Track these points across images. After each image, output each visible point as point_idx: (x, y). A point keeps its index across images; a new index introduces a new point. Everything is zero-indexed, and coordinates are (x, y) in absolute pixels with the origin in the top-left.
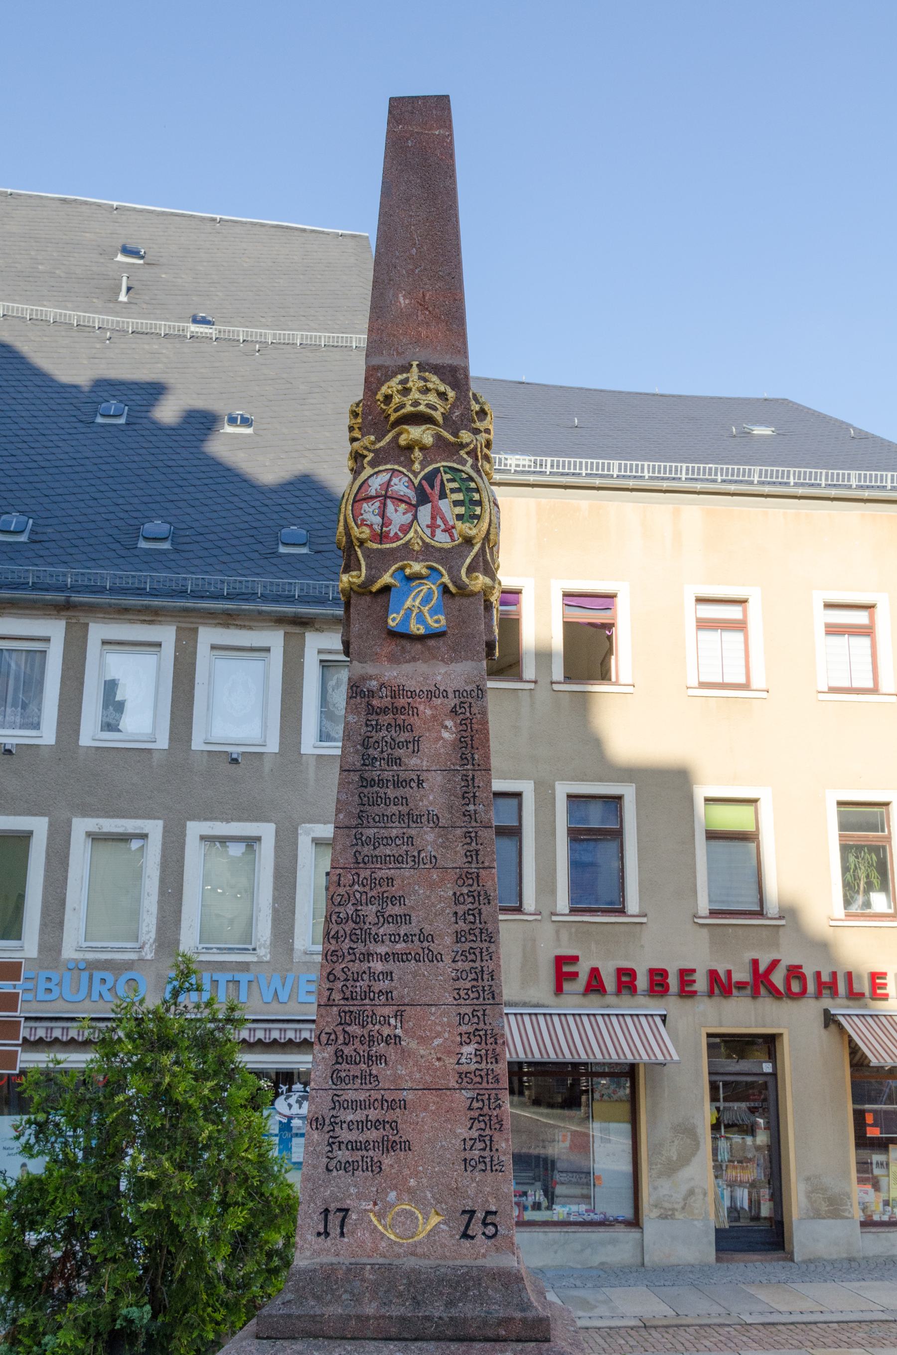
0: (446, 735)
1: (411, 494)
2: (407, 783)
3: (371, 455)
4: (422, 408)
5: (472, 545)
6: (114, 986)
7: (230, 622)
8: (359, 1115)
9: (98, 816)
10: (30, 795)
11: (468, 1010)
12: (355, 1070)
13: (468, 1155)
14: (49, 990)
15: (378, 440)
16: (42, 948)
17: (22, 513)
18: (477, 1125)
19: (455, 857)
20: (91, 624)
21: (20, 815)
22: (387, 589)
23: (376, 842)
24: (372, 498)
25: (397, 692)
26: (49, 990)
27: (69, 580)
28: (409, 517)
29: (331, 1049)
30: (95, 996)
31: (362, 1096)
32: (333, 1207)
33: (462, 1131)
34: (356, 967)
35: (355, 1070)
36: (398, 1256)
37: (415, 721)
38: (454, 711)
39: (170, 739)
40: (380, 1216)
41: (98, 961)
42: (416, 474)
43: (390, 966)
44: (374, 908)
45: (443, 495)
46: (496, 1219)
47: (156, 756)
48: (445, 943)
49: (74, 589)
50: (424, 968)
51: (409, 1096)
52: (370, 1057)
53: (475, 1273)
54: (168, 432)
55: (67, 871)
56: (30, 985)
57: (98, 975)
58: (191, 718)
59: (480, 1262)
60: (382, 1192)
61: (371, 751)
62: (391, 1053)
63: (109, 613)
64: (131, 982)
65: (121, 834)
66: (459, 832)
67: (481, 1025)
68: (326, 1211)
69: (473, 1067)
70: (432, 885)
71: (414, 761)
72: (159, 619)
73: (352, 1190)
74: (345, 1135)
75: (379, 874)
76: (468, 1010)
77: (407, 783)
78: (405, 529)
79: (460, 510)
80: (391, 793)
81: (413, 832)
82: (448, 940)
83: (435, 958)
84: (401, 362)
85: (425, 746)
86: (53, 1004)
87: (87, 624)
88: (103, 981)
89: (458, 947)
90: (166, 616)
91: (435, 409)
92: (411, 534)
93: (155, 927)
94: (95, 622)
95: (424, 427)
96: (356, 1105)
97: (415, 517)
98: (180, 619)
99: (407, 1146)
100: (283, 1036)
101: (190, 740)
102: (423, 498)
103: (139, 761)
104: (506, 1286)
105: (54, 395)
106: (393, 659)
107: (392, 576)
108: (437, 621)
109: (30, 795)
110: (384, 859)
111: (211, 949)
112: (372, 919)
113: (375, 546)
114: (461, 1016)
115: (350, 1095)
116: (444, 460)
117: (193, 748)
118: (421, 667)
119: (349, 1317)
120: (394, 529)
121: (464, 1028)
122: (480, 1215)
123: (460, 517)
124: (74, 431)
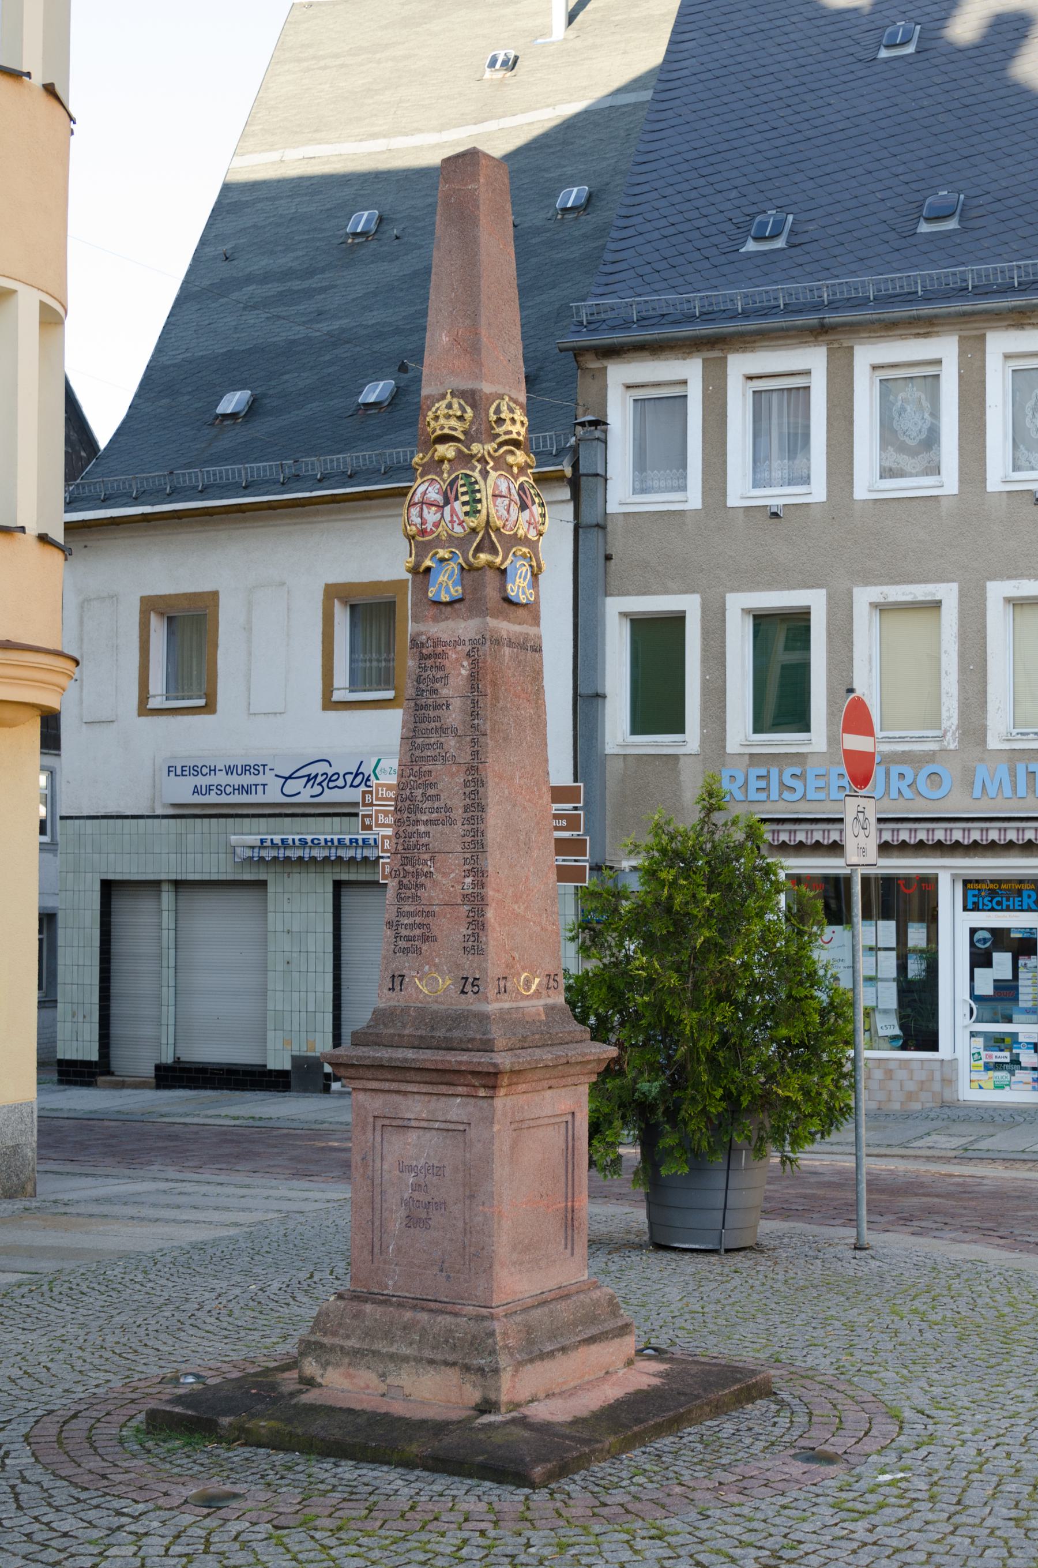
1: (440, 499)
2: (441, 706)
3: (420, 469)
4: (446, 431)
5: (478, 533)
6: (914, 782)
7: (1026, 322)
8: (411, 921)
9: (881, 584)
10: (803, 564)
11: (468, 855)
12: (409, 893)
13: (466, 944)
18: (471, 927)
19: (465, 757)
20: (856, 348)
21: (794, 588)
22: (428, 569)
24: (417, 504)
25: (437, 642)
27: (825, 295)
28: (439, 515)
29: (397, 880)
30: (894, 794)
31: (412, 909)
33: (464, 931)
34: (411, 829)
35: (409, 893)
36: (428, 1003)
37: (446, 662)
38: (468, 655)
39: (961, 481)
40: (420, 980)
41: (895, 754)
42: (444, 481)
43: (429, 828)
44: (420, 791)
45: (456, 499)
46: (479, 983)
47: (944, 502)
48: (458, 814)
49: (833, 306)
50: (447, 829)
51: (436, 909)
52: (417, 885)
53: (466, 1013)
54: (971, 53)
55: (851, 651)
56: (821, 783)
57: (895, 770)
58: (985, 451)
59: (469, 1007)
60: (421, 966)
61: (421, 685)
62: (428, 883)
63: (875, 331)
64: (933, 776)
65: (912, 603)
66: (468, 739)
67: (476, 865)
69: (471, 891)
70: (453, 775)
71: (444, 692)
72: (935, 329)
73: (407, 964)
74: (404, 932)
75: (424, 769)
76: (468, 855)
77: (441, 706)
78: (437, 525)
79: (467, 508)
80: (432, 713)
81: (442, 740)
82: (460, 811)
83: (452, 822)
84: (442, 391)
85: (451, 680)
87: (852, 348)
88: (902, 776)
89: (466, 815)
90: (942, 325)
91: (455, 429)
93: (956, 711)
94: (860, 344)
95: (447, 446)
96: (409, 914)
97: (442, 516)
98: (963, 326)
100: (1020, 837)
101: (984, 480)
102: (447, 502)
103: (925, 513)
104: (480, 1021)
105: (829, 28)
106: (435, 619)
107: (431, 559)
109: (803, 564)
111: (1028, 734)
112: (419, 798)
113: (421, 539)
114: (466, 859)
115: (406, 908)
116: (463, 468)
117: (989, 489)
118: (450, 624)
119: (395, 1035)
121: (467, 867)
122: (471, 980)
124: (851, 77)
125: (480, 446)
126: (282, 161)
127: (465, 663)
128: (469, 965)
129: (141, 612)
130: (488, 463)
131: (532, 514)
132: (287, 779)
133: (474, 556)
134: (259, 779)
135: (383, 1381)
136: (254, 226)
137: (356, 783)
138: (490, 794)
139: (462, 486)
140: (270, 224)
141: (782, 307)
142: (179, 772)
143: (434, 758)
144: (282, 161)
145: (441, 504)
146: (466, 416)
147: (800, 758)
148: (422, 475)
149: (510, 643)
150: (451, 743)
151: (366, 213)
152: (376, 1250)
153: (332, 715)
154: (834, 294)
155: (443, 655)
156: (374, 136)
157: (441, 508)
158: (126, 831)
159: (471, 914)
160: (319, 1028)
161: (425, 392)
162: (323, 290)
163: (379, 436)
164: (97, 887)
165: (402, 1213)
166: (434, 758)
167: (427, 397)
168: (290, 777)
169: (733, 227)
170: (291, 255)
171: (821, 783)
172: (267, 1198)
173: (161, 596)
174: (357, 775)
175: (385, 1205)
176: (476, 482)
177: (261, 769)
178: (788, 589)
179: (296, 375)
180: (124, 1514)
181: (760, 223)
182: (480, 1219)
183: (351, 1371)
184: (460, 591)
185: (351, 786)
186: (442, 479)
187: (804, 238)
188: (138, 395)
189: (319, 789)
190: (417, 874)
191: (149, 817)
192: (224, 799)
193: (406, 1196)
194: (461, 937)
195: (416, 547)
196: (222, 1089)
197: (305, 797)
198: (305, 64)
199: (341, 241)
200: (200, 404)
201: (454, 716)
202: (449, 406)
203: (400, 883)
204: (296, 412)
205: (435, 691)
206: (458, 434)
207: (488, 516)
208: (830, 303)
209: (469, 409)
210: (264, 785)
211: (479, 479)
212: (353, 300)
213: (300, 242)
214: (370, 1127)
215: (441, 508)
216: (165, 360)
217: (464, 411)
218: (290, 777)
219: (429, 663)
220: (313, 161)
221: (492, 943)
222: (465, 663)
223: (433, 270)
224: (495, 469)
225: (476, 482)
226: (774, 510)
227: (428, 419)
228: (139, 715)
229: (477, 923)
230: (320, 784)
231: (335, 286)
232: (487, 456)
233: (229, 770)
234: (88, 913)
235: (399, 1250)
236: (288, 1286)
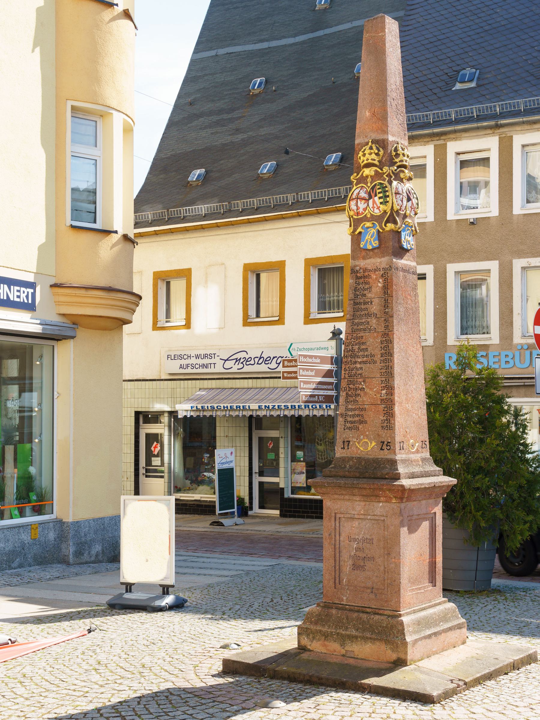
0: (379, 285)
1: (366, 196)
3: (355, 181)
4: (370, 161)
5: (387, 213)
8: (353, 413)
11: (384, 379)
12: (352, 399)
14: (507, 362)
15: (357, 175)
16: (502, 338)
17: (472, 67)
19: (381, 329)
20: (514, 136)
21: (482, 261)
22: (360, 233)
23: (358, 324)
25: (365, 270)
26: (507, 362)
27: (498, 109)
28: (366, 204)
32: (345, 440)
33: (382, 418)
34: (352, 366)
35: (352, 399)
37: (370, 280)
38: (382, 276)
40: (358, 443)
42: (369, 187)
43: (362, 366)
44: (357, 347)
45: (376, 195)
48: (378, 358)
50: (372, 366)
55: (512, 292)
56: (496, 360)
62: (362, 394)
66: (383, 319)
68: (344, 442)
71: (369, 295)
74: (349, 419)
75: (359, 335)
76: (384, 379)
78: (365, 209)
79: (382, 200)
80: (363, 307)
81: (369, 320)
82: (379, 356)
83: (375, 362)
84: (366, 141)
86: (511, 370)
89: (382, 359)
91: (374, 160)
92: (367, 211)
94: (516, 134)
96: (352, 410)
97: (368, 205)
99: (366, 422)
102: (370, 197)
106: (364, 258)
108: (376, 244)
110: (360, 330)
112: (356, 350)
120: (361, 210)
121: (383, 385)
122: (386, 443)
123: (381, 203)
125: (387, 168)
126: (216, 55)
127: (381, 280)
128: (385, 435)
129: (154, 279)
130: (392, 177)
131: (412, 204)
132: (226, 360)
133: (385, 225)
134: (212, 361)
135: (343, 648)
136: (204, 88)
137: (259, 362)
138: (395, 347)
139: (378, 189)
140: (212, 87)
141: (475, 117)
142: (173, 358)
143: (364, 330)
144: (216, 55)
145: (367, 199)
146: (380, 153)
147: (485, 347)
148: (356, 185)
149: (404, 271)
150: (373, 322)
151: (259, 79)
152: (337, 581)
153: (248, 328)
154: (503, 109)
155: (369, 276)
156: (262, 41)
157: (367, 201)
158: (147, 387)
159: (385, 409)
160: (242, 484)
161: (357, 142)
162: (240, 118)
163: (269, 190)
164: (133, 415)
165: (350, 562)
166: (364, 330)
167: (359, 144)
168: (227, 360)
169: (448, 77)
170: (223, 101)
171: (496, 360)
172: (234, 564)
173: (163, 271)
174: (260, 358)
175: (341, 559)
176: (386, 187)
177: (213, 356)
178: (479, 261)
179: (227, 160)
180: (227, 711)
181: (462, 75)
182: (393, 565)
183: (326, 643)
184: (378, 243)
185: (258, 364)
186: (367, 186)
187: (486, 82)
188: (150, 173)
189: (241, 366)
190: (357, 389)
191: (158, 380)
192: (195, 371)
193: (352, 554)
194: (380, 422)
195: (354, 221)
196: (194, 514)
197: (235, 370)
198: (227, 6)
199: (247, 93)
200: (180, 177)
201: (375, 307)
202: (371, 148)
203: (347, 394)
204: (228, 179)
205: (364, 295)
206: (376, 162)
207: (393, 204)
208: (501, 113)
209: (381, 149)
210: (214, 364)
211: (387, 185)
212: (254, 123)
213: (227, 95)
214: (333, 519)
215: (367, 201)
216: (162, 155)
217: (379, 150)
218: (227, 360)
219: (361, 281)
220: (232, 55)
221: (397, 424)
222: (381, 280)
223: (361, 79)
224: (395, 179)
225: (386, 187)
226: (472, 221)
227: (359, 155)
228: (153, 330)
229: (389, 414)
230: (242, 363)
231: (244, 116)
232: (391, 173)
233: (197, 357)
234: (129, 428)
235: (349, 581)
236: (262, 605)
